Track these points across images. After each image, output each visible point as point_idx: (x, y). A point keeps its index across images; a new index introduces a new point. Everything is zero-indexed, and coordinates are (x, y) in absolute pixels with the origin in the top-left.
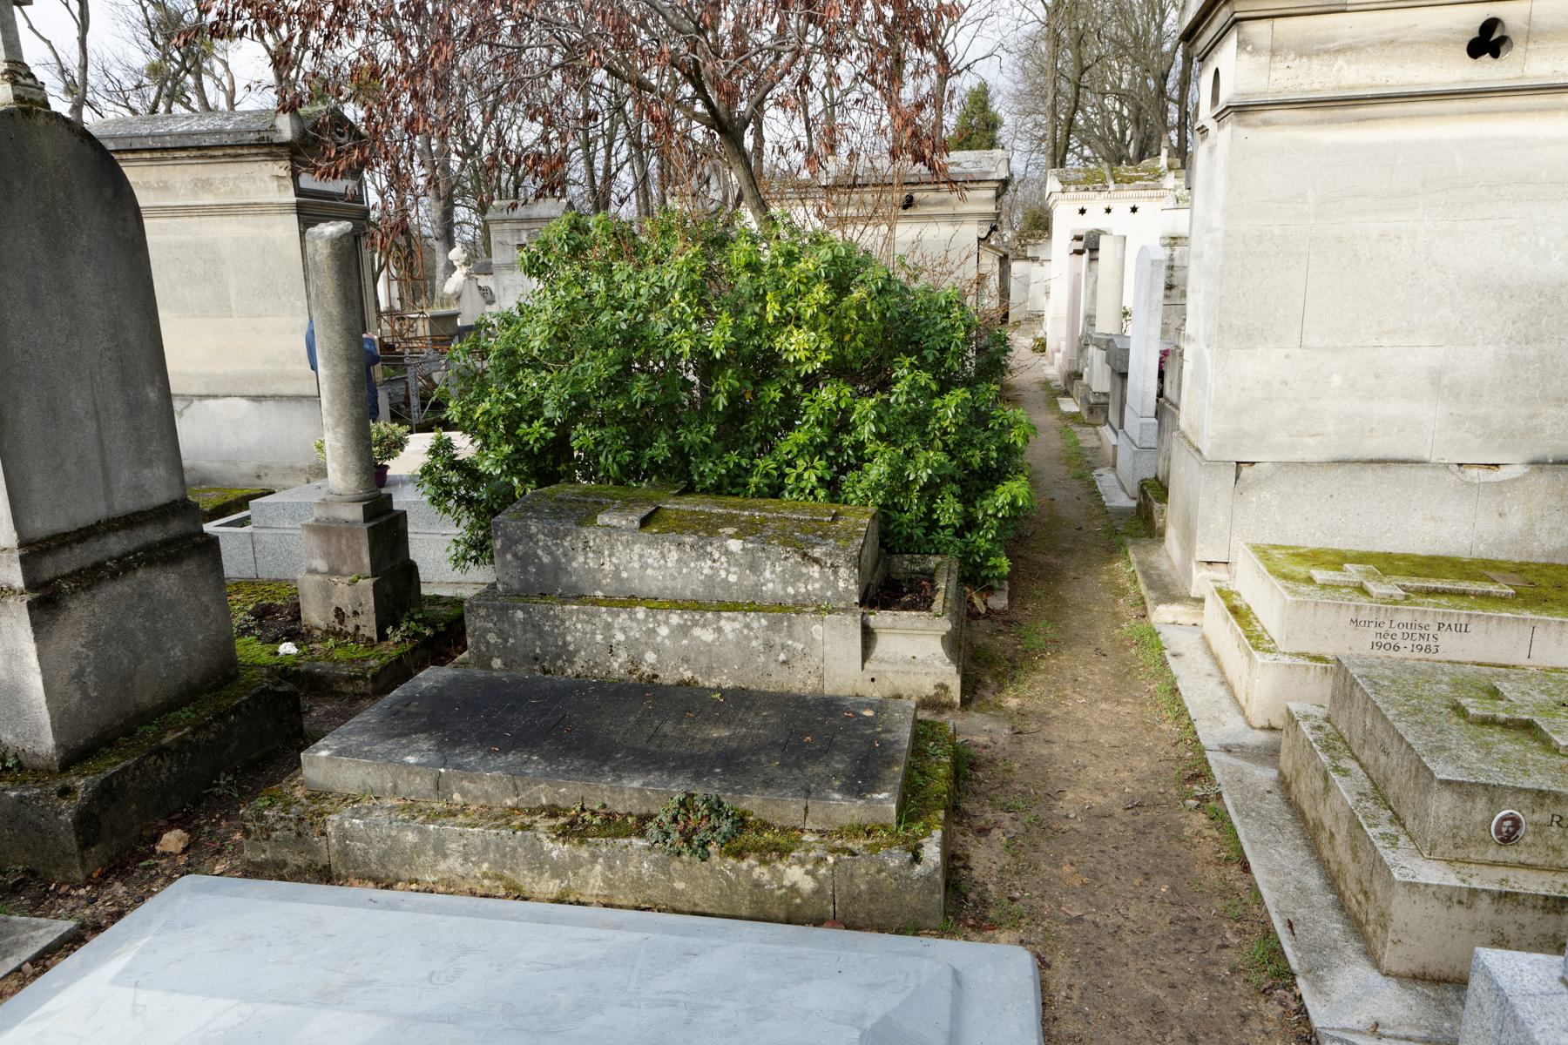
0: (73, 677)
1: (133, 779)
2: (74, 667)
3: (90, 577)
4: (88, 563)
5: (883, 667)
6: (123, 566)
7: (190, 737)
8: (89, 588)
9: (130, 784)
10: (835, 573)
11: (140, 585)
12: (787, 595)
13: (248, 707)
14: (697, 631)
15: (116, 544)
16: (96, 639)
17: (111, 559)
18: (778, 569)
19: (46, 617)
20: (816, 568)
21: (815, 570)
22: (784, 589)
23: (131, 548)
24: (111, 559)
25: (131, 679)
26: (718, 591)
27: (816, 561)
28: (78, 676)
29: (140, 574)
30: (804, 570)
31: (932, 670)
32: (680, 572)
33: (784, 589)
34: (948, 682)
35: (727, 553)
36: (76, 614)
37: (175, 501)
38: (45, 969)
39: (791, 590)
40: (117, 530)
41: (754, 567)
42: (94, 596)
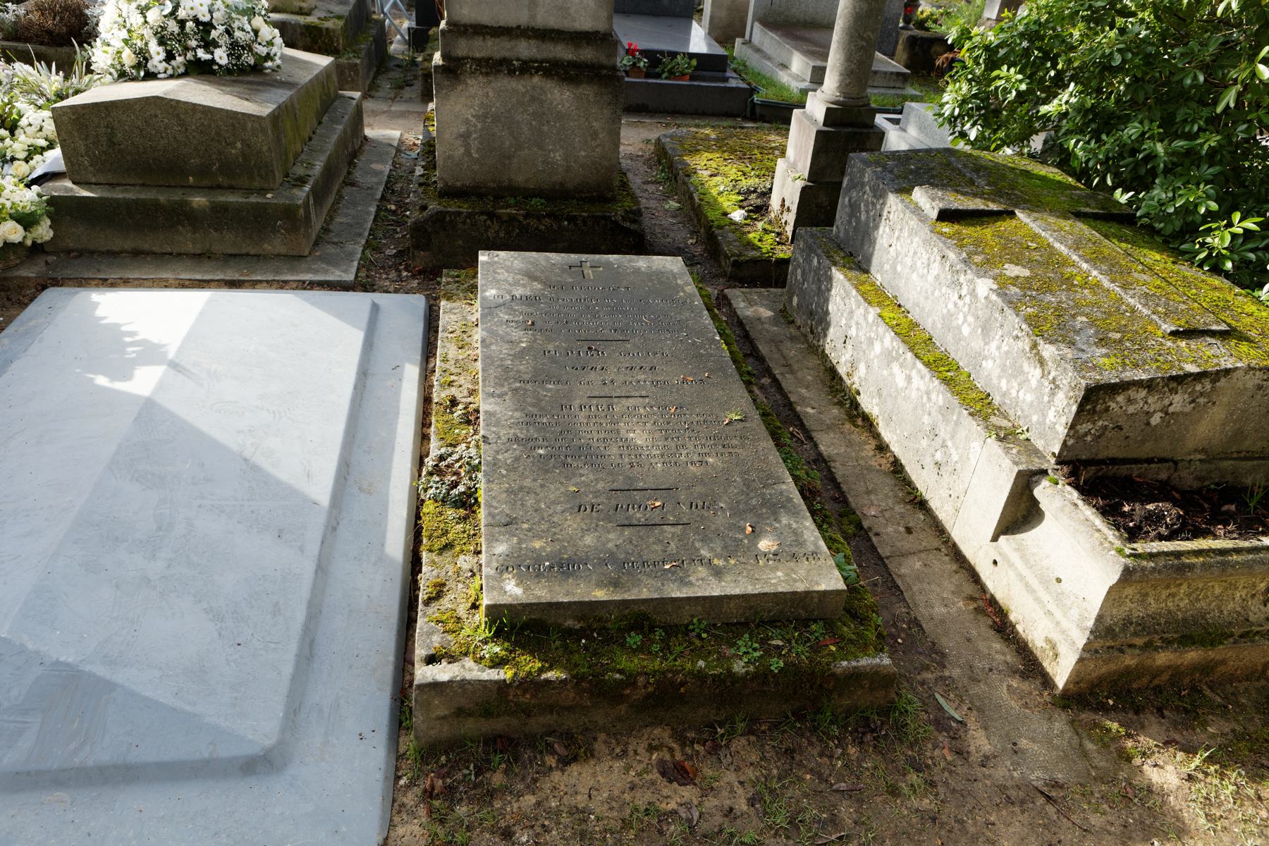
0: (461, 136)
1: (464, 223)
2: (463, 129)
3: (493, 67)
4: (497, 56)
5: (1015, 558)
6: (526, 68)
7: (521, 218)
8: (487, 74)
9: (460, 226)
10: (1053, 394)
11: (534, 88)
12: (999, 388)
13: (584, 222)
14: (895, 367)
15: (525, 49)
16: (485, 116)
17: (518, 60)
18: (1005, 348)
19: (447, 83)
20: (1038, 372)
21: (1035, 373)
22: (1000, 378)
23: (539, 57)
24: (518, 60)
25: (509, 158)
26: (950, 337)
27: (1042, 362)
28: (465, 137)
29: (536, 79)
30: (1026, 366)
31: (1059, 615)
32: (933, 294)
33: (1000, 378)
34: (1062, 649)
35: (973, 293)
36: (472, 90)
37: (597, 32)
38: (312, 289)
39: (1003, 384)
40: (529, 38)
41: (986, 330)
42: (490, 82)
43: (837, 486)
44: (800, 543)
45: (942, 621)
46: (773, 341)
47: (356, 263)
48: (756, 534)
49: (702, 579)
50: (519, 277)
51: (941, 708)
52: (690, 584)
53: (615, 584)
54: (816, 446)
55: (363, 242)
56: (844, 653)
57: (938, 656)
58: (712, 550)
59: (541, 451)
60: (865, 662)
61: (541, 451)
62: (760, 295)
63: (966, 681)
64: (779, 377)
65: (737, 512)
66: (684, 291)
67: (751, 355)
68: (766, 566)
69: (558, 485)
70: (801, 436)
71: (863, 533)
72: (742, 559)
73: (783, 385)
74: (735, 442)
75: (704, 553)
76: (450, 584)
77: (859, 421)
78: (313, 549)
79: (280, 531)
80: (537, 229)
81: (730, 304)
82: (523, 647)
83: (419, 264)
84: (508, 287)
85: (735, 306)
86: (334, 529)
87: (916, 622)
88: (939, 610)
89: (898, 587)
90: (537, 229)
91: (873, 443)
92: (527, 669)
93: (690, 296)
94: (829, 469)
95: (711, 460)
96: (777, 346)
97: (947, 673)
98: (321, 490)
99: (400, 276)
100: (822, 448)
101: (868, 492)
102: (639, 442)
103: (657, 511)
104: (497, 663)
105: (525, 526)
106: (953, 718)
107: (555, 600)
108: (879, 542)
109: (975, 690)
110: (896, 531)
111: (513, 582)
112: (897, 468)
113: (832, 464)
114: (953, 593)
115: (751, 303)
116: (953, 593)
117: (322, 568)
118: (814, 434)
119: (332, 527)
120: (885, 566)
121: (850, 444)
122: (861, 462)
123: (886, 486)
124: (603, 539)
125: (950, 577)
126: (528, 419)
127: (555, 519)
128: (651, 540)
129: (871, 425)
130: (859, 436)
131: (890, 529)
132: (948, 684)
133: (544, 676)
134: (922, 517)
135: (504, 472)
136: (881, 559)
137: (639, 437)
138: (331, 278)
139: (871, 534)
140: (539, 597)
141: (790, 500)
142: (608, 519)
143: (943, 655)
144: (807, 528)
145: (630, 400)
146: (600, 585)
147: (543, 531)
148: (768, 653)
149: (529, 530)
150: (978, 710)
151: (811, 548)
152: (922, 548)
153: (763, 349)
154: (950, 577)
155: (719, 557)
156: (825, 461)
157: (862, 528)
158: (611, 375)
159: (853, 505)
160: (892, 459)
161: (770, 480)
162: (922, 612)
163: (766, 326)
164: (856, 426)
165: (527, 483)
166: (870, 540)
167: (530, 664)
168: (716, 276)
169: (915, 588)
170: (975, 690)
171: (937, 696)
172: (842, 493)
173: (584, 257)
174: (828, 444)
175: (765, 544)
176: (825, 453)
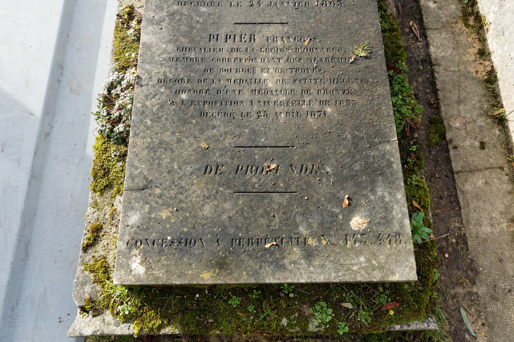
43: (435, 91)
44: (387, 221)
45: (485, 240)
48: (352, 208)
49: (295, 262)
51: (461, 321)
52: (282, 268)
53: (221, 265)
54: (427, 45)
56: (398, 318)
57: (472, 272)
58: (309, 226)
59: (184, 96)
60: (415, 326)
61: (184, 96)
63: (487, 298)
65: (341, 180)
68: (353, 248)
69: (192, 140)
70: (417, 33)
71: (444, 143)
72: (333, 240)
74: (355, 86)
75: (303, 230)
76: (106, 228)
77: (471, 22)
78: (28, 160)
79: (3, 144)
82: (150, 304)
86: (48, 135)
87: (463, 239)
88: (486, 229)
89: (458, 202)
91: (477, 46)
92: (150, 325)
94: (432, 72)
95: (329, 110)
97: (475, 290)
98: (35, 101)
100: (432, 49)
101: (459, 102)
102: (270, 85)
103: (271, 175)
104: (128, 319)
105: (158, 191)
106: (468, 331)
107: (169, 282)
108: (455, 155)
109: (493, 308)
110: (472, 146)
111: (138, 260)
112: (491, 79)
113: (436, 68)
114: (501, 213)
116: (501, 213)
117: (36, 178)
118: (429, 33)
119: (45, 134)
120: (454, 180)
121: (457, 45)
122: (462, 67)
123: (475, 95)
124: (220, 209)
125: (504, 196)
126: (179, 54)
127: (183, 183)
128: (260, 211)
129: (481, 27)
130: (467, 37)
131: (468, 143)
132: (473, 298)
133: (163, 332)
134: (497, 132)
135: (149, 123)
136: (452, 172)
137: (270, 78)
139: (450, 147)
140: (157, 278)
141: (390, 164)
142: (227, 184)
143: (477, 272)
144: (397, 201)
145: (272, 28)
146: (209, 266)
147: (171, 198)
148: (337, 317)
149: (160, 196)
150: (489, 326)
151: (396, 227)
152: (488, 165)
154: (504, 196)
155: (313, 235)
156: (431, 64)
157: (444, 138)
159: (443, 115)
160: (489, 69)
161: (379, 136)
162: (471, 230)
164: (467, 25)
165: (167, 137)
166: (448, 151)
167: (153, 322)
169: (472, 206)
170: (493, 308)
171: (462, 310)
172: (437, 99)
174: (439, 46)
175: (357, 222)
176: (433, 55)
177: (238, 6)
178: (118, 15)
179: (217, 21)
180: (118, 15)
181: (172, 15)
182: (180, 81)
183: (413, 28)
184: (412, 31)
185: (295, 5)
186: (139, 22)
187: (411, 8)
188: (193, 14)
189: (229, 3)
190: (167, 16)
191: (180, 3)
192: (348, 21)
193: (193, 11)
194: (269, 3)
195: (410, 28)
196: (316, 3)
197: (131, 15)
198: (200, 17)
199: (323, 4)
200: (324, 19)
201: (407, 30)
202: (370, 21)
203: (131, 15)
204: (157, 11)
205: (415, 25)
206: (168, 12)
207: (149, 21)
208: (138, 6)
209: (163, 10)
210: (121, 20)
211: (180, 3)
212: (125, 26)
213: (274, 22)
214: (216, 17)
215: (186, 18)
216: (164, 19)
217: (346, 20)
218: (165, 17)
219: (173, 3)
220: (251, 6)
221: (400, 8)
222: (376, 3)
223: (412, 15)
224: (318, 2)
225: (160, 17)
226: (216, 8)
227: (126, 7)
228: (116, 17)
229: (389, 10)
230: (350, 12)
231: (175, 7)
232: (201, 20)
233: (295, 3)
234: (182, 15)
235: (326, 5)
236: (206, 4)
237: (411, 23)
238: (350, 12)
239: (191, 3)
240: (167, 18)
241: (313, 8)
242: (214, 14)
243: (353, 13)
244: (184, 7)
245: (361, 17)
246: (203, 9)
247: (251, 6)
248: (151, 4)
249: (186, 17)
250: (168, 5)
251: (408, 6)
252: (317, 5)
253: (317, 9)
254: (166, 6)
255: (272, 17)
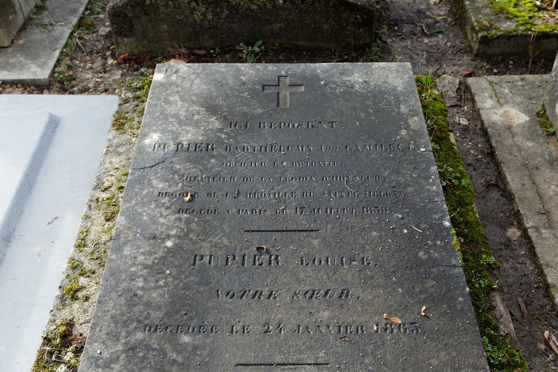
9: (162, 9)
46: (526, 165)
47: (57, 54)
50: (196, 108)
55: (75, 21)
62: (513, 86)
64: (532, 233)
66: (408, 127)
67: (496, 185)
73: (538, 250)
80: (248, 9)
81: (473, 101)
83: (124, 51)
84: (175, 127)
85: (479, 105)
90: (248, 9)
93: (415, 135)
96: (531, 177)
99: (104, 65)
115: (500, 100)
138: (25, 76)
153: (514, 180)
158: (280, 312)
163: (519, 139)
168: (460, 51)
173: (285, 68)
177: (244, 332)
178: (45, 338)
179: (207, 360)
180: (45, 338)
181: (132, 349)
182: (164, 195)
183: (551, 343)
184: (551, 349)
185: (340, 332)
186: (78, 352)
187: (542, 307)
188: (168, 348)
189: (229, 327)
190: (124, 352)
191: (147, 328)
192: (432, 361)
193: (169, 342)
194: (296, 328)
195: (546, 343)
196: (375, 328)
197: (67, 337)
198: (179, 352)
199: (386, 329)
200: (389, 357)
201: (542, 346)
202: (471, 361)
203: (67, 337)
204: (109, 342)
205: (554, 338)
206: (126, 343)
207: (93, 360)
208: (81, 322)
209: (118, 340)
210: (48, 348)
211: (147, 328)
212: (54, 358)
213: (304, 361)
214: (206, 353)
215: (155, 356)
216: (118, 358)
217: (429, 359)
218: (120, 353)
219: (136, 328)
220: (266, 332)
221: (523, 306)
222: (477, 328)
223: (546, 319)
224: (377, 325)
225: (112, 353)
226: (207, 337)
227: (62, 324)
228: (41, 341)
229: (502, 326)
230: (434, 344)
231: (139, 335)
232: (180, 359)
233: (340, 327)
234: (148, 350)
235: (392, 332)
236: (191, 330)
237: (546, 333)
238: (434, 344)
239: (167, 328)
240: (123, 356)
241: (370, 335)
242: (203, 348)
243: (440, 346)
244: (154, 336)
245: (454, 354)
246: (186, 339)
247: (266, 332)
248: (100, 331)
249: (155, 353)
250: (127, 332)
251: (537, 304)
252: (377, 331)
253: (376, 338)
254: (124, 334)
255: (301, 353)
